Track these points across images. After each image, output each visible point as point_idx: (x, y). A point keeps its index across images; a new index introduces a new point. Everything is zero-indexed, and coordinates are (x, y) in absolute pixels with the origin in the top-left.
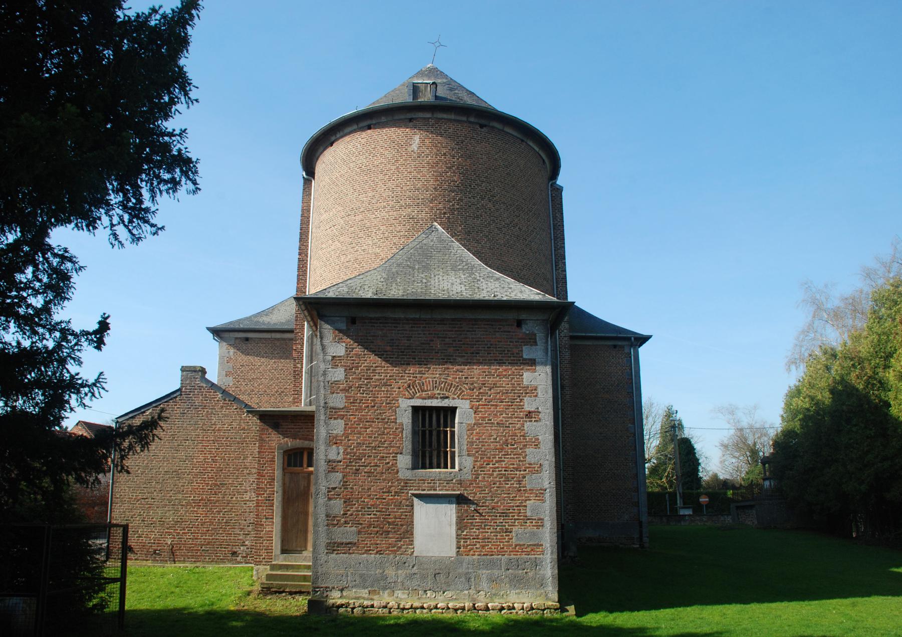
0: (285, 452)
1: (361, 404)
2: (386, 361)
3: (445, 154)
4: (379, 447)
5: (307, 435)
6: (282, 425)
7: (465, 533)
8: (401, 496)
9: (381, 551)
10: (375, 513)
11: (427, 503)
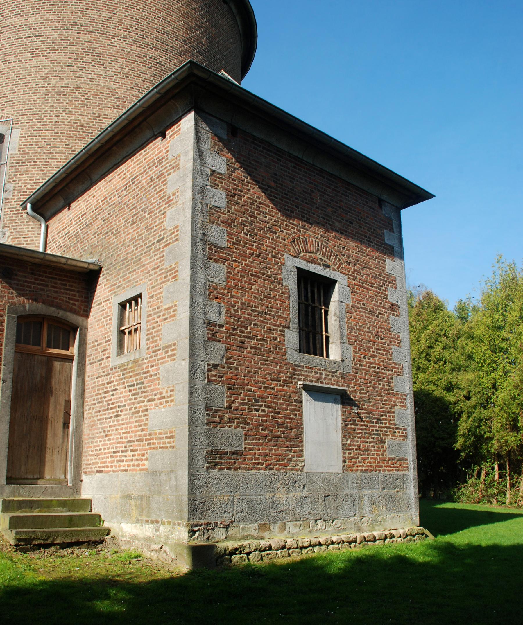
0: (19, 317)
1: (245, 249)
2: (271, 200)
3: (195, 9)
4: (265, 314)
5: (54, 298)
6: (16, 275)
7: (349, 442)
8: (289, 387)
9: (271, 464)
10: (263, 408)
11: (316, 400)
